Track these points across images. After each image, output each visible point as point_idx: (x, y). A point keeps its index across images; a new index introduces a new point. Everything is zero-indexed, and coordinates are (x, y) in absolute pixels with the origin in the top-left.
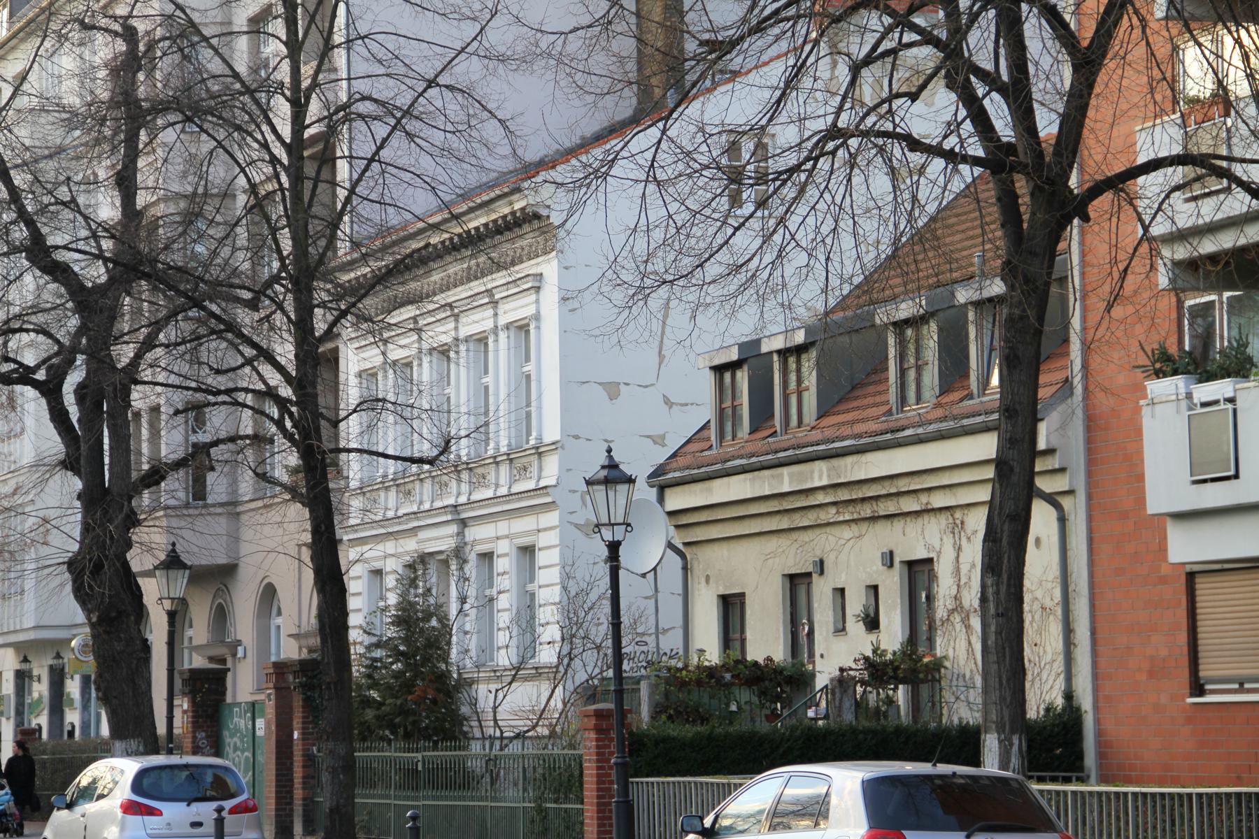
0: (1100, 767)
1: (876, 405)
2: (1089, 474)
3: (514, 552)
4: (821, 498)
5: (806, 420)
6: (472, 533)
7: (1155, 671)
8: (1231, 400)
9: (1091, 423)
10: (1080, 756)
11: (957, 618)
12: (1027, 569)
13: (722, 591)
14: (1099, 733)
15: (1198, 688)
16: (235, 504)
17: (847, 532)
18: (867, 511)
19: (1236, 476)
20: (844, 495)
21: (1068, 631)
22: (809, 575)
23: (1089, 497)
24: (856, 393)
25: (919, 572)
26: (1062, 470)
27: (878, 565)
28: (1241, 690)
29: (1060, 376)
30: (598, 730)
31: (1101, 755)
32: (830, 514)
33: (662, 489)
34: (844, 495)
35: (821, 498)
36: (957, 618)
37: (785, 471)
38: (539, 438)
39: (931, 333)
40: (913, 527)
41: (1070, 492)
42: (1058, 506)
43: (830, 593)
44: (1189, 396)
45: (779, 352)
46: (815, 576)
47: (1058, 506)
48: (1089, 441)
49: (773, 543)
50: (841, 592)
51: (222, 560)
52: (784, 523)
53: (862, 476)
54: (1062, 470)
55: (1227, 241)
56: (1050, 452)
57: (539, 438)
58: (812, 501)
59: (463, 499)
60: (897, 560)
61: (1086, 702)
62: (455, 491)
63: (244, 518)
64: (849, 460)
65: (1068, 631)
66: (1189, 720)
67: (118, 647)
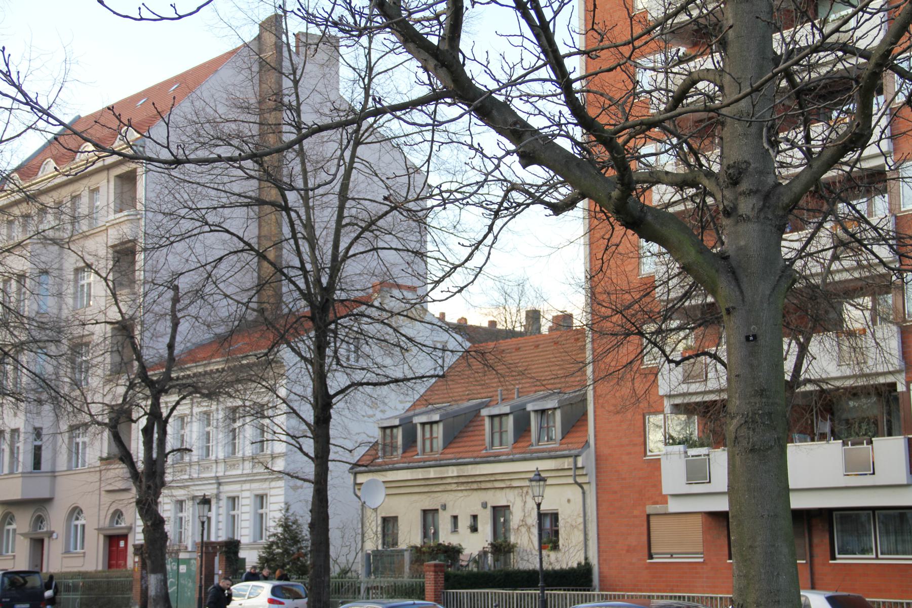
0: (600, 585)
1: (480, 445)
2: (597, 477)
3: (253, 497)
4: (449, 481)
6: (224, 488)
7: (630, 550)
8: (708, 455)
9: (598, 458)
11: (523, 530)
12: (331, 511)
14: (600, 573)
15: (651, 557)
16: (54, 472)
18: (475, 486)
20: (462, 480)
21: (586, 534)
22: (437, 510)
24: (457, 440)
25: (499, 512)
26: (586, 475)
27: (480, 507)
28: (672, 557)
29: (584, 440)
30: (435, 572)
31: (601, 581)
32: (454, 487)
33: (355, 474)
34: (462, 480)
36: (523, 530)
37: (432, 469)
39: (510, 422)
40: (499, 493)
41: (589, 483)
42: (582, 488)
44: (686, 452)
46: (440, 511)
47: (582, 488)
48: (597, 464)
49: (423, 497)
50: (455, 518)
53: (478, 473)
54: (586, 475)
55: (698, 399)
56: (582, 468)
58: (444, 481)
60: (489, 506)
64: (470, 467)
65: (586, 534)
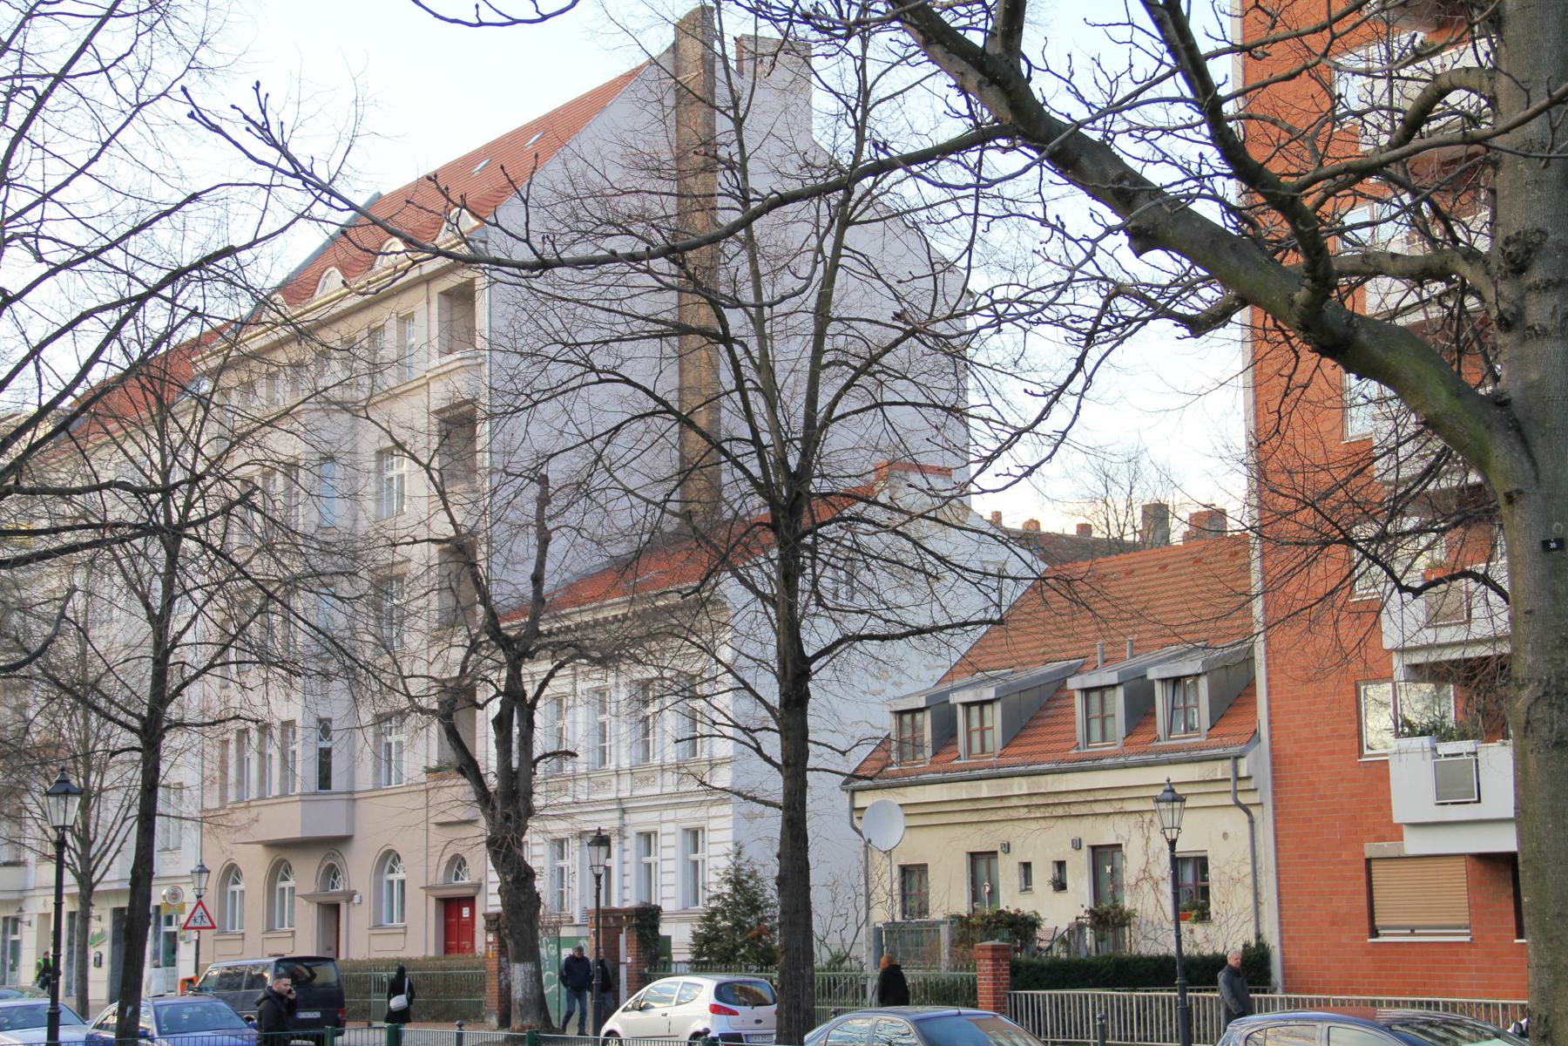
0: (1285, 982)
3: (680, 832)
4: (1015, 802)
5: (989, 748)
6: (631, 818)
8: (1475, 753)
10: (1268, 974)
11: (1146, 886)
13: (903, 862)
14: (1284, 961)
17: (1034, 825)
18: (1059, 811)
19: (1479, 801)
20: (1036, 800)
22: (995, 853)
23: (1275, 807)
26: (1255, 790)
28: (1412, 933)
31: (1285, 975)
32: (1023, 813)
34: (1036, 800)
35: (1015, 802)
36: (1146, 886)
37: (984, 783)
38: (711, 754)
40: (1101, 824)
42: (1249, 813)
43: (1016, 866)
44: (1435, 749)
45: (963, 704)
47: (1249, 813)
50: (1027, 866)
51: (342, 832)
52: (975, 817)
54: (1255, 790)
55: (1456, 654)
57: (711, 754)
58: (1007, 803)
59: (626, 794)
60: (1084, 845)
61: (1272, 940)
62: (614, 788)
63: (359, 803)
64: (1050, 777)
66: (1368, 953)
67: (523, 898)
